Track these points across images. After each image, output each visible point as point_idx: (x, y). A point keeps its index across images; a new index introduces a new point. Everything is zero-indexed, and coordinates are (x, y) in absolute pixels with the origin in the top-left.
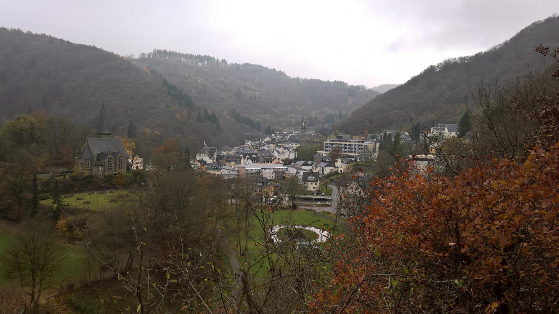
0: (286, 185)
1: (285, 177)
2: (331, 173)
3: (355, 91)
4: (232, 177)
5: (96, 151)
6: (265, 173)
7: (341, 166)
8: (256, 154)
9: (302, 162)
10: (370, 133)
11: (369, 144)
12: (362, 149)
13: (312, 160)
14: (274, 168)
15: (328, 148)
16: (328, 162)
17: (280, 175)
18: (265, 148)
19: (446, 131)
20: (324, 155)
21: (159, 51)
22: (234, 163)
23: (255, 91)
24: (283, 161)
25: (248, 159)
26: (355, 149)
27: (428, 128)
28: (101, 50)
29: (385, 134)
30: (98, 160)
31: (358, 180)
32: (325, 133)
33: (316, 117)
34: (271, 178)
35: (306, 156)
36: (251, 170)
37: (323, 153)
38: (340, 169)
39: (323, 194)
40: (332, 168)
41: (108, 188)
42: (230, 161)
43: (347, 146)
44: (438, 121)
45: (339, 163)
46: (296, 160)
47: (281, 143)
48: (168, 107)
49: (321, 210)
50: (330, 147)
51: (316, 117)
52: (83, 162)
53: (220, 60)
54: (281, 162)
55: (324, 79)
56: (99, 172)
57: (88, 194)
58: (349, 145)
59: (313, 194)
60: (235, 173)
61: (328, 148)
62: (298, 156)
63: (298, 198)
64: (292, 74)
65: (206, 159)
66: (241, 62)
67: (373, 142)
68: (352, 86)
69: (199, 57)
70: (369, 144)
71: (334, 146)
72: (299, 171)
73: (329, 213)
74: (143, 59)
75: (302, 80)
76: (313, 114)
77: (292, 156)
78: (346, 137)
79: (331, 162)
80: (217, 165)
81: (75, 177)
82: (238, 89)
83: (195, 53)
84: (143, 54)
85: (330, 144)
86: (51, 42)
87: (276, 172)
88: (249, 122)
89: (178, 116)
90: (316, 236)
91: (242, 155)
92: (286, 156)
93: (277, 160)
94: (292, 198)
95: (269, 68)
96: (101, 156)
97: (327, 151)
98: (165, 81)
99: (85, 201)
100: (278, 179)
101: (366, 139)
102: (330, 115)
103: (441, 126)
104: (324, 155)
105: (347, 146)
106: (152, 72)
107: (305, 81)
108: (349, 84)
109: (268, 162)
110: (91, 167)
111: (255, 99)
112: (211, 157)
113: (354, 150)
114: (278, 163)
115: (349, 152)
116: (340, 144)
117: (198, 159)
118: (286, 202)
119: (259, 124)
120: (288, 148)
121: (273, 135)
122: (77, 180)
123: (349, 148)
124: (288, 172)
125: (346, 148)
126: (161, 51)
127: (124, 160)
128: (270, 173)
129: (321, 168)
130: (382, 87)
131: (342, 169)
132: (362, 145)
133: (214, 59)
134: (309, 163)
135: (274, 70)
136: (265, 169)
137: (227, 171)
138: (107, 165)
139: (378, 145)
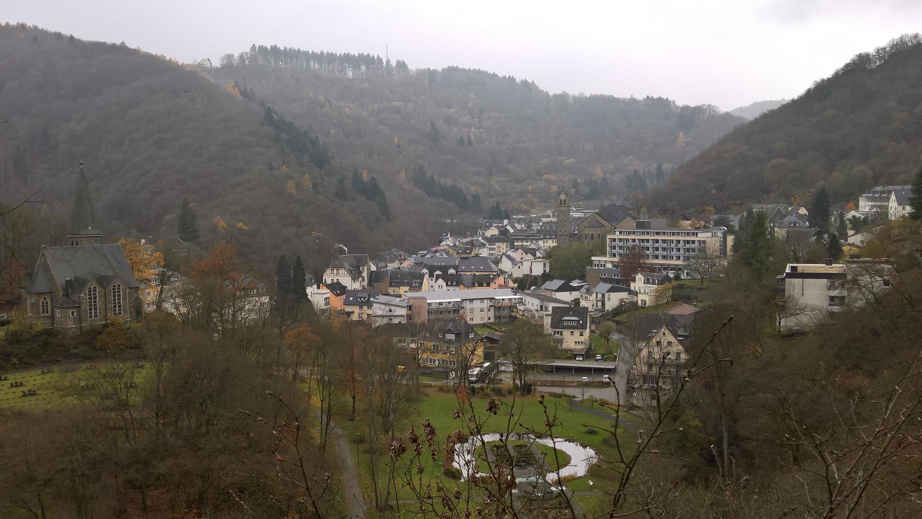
0: (512, 335)
1: (516, 317)
2: (620, 306)
3: (692, 117)
4: (396, 321)
5: (62, 274)
6: (472, 311)
7: (644, 290)
8: (456, 268)
9: (557, 283)
10: (718, 211)
11: (711, 239)
12: (693, 250)
13: (582, 278)
14: (491, 299)
15: (617, 250)
16: (617, 281)
17: (505, 313)
18: (484, 253)
19: (893, 204)
20: (609, 266)
21: (262, 49)
22: (407, 288)
23: (470, 126)
24: (515, 281)
25: (438, 277)
26: (679, 250)
27: (850, 197)
28: (136, 53)
29: (750, 213)
30: (67, 295)
31: (672, 324)
32: (612, 216)
33: (604, 180)
34: (486, 320)
35: (569, 268)
36: (440, 304)
37: (606, 261)
38: (641, 297)
39: (599, 357)
40: (624, 295)
41: (86, 358)
42: (399, 285)
43: (660, 244)
44: (876, 181)
45: (638, 283)
46: (546, 277)
47: (522, 240)
48: (271, 168)
49: (586, 397)
50: (621, 248)
51: (604, 180)
52: (33, 300)
53: (393, 63)
54: (511, 284)
55: (622, 92)
56: (67, 321)
57: (39, 372)
58: (664, 241)
59: (574, 357)
60: (403, 312)
61: (617, 250)
62: (551, 268)
63: (532, 367)
64: (551, 86)
65: (346, 280)
66: (439, 65)
67: (720, 234)
68: (685, 108)
69: (347, 59)
70: (711, 239)
71: (630, 243)
72: (546, 304)
73: (603, 403)
74: (229, 67)
75: (574, 98)
76: (598, 172)
77: (538, 269)
78: (662, 221)
79: (622, 282)
80: (366, 295)
81: (15, 333)
82: (432, 124)
83: (340, 51)
84: (230, 57)
85: (620, 240)
86: (35, 38)
87: (498, 307)
88: (454, 194)
89: (291, 187)
90: (562, 460)
91: (425, 271)
92: (525, 270)
93: (501, 280)
94: (521, 369)
95: (501, 76)
96: (71, 287)
97: (614, 255)
98: (269, 112)
99: (26, 389)
100: (500, 324)
101: (706, 228)
102: (635, 172)
103: (881, 192)
104: (609, 266)
105: (660, 244)
106: (244, 93)
107: (581, 101)
108: (680, 104)
109: (481, 285)
110: (53, 312)
111: (470, 143)
112: (355, 275)
113: (674, 253)
114: (504, 286)
115: (664, 257)
116: (643, 241)
117: (329, 282)
118: (507, 377)
119: (476, 197)
120: (533, 252)
121: (506, 222)
122: (19, 342)
123: (664, 249)
124: (521, 308)
125: (657, 249)
126: (266, 48)
127: (125, 294)
128: (482, 310)
129: (600, 296)
130: (755, 105)
131: (646, 298)
132: (693, 242)
133: (380, 60)
134: (574, 284)
135: (512, 80)
136: (471, 300)
137: (388, 308)
138: (85, 306)
139: (730, 239)
